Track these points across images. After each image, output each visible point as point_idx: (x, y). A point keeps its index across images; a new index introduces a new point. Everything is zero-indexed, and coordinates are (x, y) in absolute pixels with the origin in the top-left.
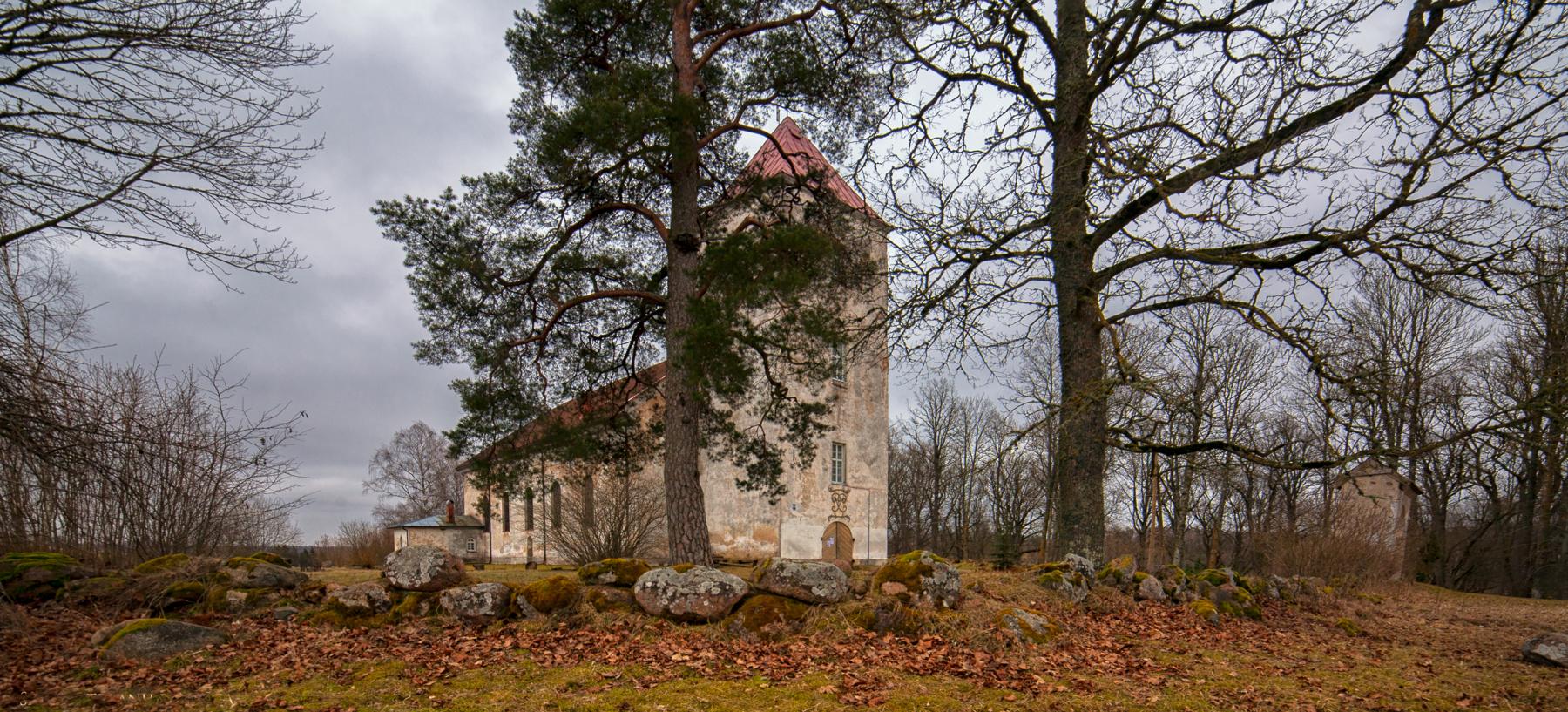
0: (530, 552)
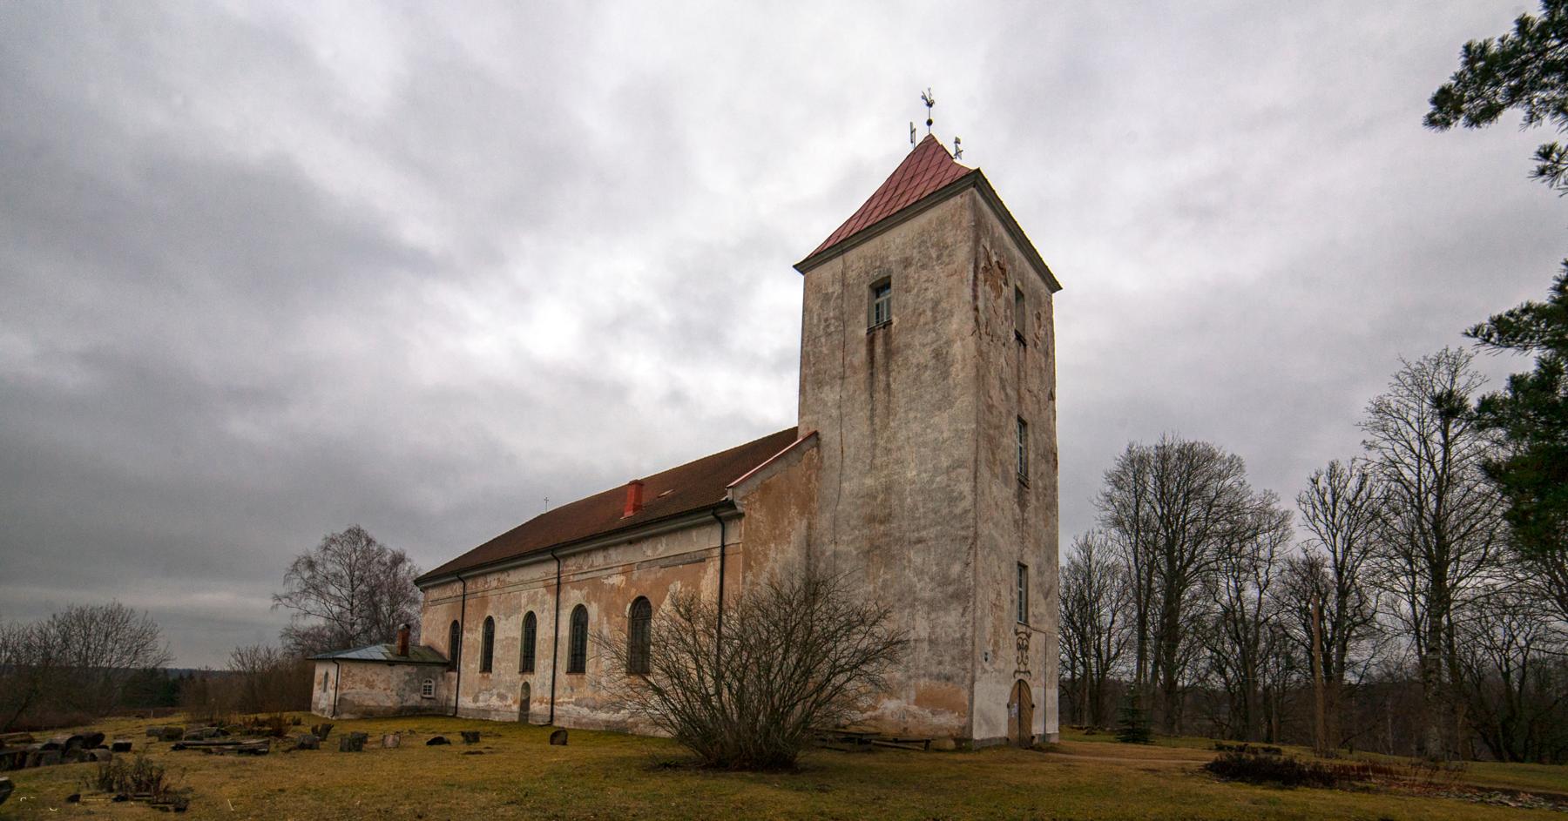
0: (525, 704)
